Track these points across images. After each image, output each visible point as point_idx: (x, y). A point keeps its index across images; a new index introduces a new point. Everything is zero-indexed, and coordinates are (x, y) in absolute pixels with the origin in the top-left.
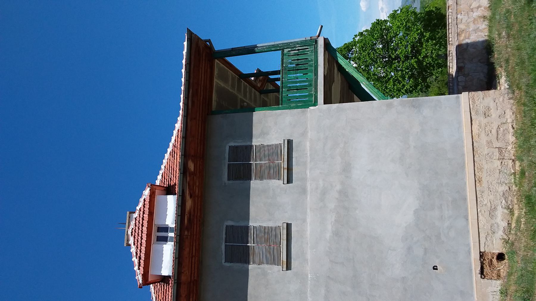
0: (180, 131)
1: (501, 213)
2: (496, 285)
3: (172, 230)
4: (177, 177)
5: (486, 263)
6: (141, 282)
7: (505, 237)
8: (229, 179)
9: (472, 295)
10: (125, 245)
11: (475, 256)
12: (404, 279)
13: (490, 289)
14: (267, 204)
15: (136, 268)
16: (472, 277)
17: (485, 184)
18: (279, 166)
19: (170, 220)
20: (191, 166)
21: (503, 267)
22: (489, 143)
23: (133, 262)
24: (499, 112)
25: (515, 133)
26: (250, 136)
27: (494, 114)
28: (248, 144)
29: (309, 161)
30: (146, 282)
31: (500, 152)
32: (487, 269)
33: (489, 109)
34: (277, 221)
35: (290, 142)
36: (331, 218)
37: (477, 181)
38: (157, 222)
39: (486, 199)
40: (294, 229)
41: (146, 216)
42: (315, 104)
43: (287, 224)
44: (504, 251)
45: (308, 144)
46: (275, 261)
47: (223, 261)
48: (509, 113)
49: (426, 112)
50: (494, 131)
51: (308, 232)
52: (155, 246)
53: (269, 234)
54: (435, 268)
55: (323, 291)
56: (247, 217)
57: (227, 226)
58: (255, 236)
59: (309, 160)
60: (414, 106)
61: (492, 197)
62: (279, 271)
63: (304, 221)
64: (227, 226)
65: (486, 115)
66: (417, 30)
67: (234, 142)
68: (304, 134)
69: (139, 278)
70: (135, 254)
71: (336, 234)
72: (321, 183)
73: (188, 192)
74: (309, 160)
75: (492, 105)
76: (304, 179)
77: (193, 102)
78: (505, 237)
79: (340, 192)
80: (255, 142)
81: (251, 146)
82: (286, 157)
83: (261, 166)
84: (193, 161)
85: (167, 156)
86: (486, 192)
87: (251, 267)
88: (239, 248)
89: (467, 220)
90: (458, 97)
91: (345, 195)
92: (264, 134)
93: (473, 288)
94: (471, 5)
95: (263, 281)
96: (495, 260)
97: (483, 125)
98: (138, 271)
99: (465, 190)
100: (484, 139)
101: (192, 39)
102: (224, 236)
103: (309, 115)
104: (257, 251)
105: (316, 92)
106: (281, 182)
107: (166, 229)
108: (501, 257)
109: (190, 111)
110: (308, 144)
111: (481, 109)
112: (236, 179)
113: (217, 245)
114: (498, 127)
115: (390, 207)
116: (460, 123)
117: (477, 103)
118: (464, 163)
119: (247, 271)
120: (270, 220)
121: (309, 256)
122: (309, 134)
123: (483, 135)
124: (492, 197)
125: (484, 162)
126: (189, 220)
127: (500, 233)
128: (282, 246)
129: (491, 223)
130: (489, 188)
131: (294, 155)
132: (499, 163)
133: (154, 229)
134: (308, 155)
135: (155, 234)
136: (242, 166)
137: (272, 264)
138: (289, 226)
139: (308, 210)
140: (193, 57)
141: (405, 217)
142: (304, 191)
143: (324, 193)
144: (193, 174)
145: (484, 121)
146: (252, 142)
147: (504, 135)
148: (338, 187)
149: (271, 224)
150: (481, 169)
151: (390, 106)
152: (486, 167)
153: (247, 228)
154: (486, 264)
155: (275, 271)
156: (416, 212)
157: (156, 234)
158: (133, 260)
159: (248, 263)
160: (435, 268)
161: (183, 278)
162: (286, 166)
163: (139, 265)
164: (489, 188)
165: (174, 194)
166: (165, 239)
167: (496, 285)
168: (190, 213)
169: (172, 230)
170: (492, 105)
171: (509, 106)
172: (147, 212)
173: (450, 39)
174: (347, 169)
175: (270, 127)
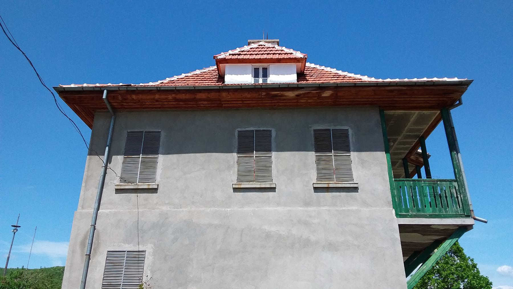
6: (219, 57)
8: (315, 131)
10: (249, 41)
14: (293, 168)
15: (230, 52)
18: (330, 179)
20: (327, 94)
23: (235, 49)
26: (359, 149)
28: (352, 148)
29: (337, 209)
30: (219, 62)
35: (355, 189)
38: (272, 67)
40: (271, 194)
41: (277, 56)
42: (398, 215)
43: (275, 188)
45: (354, 208)
47: (239, 130)
51: (268, 208)
52: (250, 67)
55: (216, 222)
57: (270, 131)
62: (232, 181)
63: (279, 204)
64: (270, 131)
67: (352, 134)
68: (365, 204)
69: (222, 56)
70: (242, 50)
71: (268, 236)
72: (316, 221)
73: (302, 92)
80: (354, 155)
82: (340, 186)
83: (330, 161)
84: (332, 95)
85: (334, 71)
87: (235, 155)
88: (253, 143)
91: (306, 244)
92: (363, 163)
98: (228, 54)
102: (261, 129)
103: (386, 208)
104: (247, 160)
110: (354, 208)
119: (229, 151)
121: (246, 209)
126: (276, 96)
128: (255, 184)
131: (343, 194)
133: (265, 65)
134: (344, 208)
135: (260, 66)
139: (289, 208)
140: (441, 88)
142: (307, 203)
143: (307, 224)
144: (319, 96)
146: (354, 151)
148: (313, 238)
159: (238, 153)
161: (224, 94)
162: (331, 186)
163: (233, 55)
168: (282, 96)
174: (332, 247)
175: (371, 169)
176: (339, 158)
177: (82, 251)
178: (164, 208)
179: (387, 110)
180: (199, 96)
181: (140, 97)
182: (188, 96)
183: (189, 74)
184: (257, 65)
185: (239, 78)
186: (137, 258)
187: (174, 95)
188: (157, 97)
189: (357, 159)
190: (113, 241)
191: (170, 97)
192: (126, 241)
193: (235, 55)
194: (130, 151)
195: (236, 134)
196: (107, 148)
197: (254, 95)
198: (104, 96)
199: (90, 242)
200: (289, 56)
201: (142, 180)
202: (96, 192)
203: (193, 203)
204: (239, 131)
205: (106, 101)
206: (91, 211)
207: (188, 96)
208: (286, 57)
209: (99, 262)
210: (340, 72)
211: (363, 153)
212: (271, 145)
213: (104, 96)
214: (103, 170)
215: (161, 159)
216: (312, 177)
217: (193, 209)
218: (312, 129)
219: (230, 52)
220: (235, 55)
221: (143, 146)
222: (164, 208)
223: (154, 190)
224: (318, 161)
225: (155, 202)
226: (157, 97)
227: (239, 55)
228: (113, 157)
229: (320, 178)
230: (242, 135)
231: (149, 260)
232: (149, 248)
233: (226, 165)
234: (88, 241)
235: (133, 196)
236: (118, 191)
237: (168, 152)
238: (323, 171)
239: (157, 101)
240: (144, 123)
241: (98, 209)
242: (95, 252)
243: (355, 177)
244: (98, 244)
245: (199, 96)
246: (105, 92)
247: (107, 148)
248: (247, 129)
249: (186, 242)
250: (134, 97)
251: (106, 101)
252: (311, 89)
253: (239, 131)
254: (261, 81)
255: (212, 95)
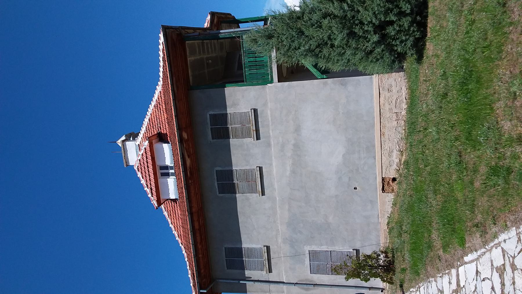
1: (395, 155)
2: (391, 197)
3: (171, 168)
5: (386, 183)
7: (398, 168)
9: (377, 202)
10: (125, 166)
11: (379, 180)
12: (336, 196)
13: (387, 199)
14: (243, 155)
15: (150, 195)
17: (386, 136)
19: (168, 161)
20: (185, 135)
21: (395, 186)
22: (391, 109)
24: (398, 88)
25: (407, 103)
27: (394, 90)
28: (224, 112)
29: (271, 124)
31: (397, 116)
32: (386, 187)
33: (391, 86)
34: (253, 165)
35: (255, 111)
37: (382, 134)
38: (159, 163)
39: (386, 147)
40: (264, 170)
41: (150, 161)
42: (271, 82)
43: (260, 167)
45: (269, 112)
46: (253, 191)
48: (404, 89)
49: (350, 88)
50: (394, 102)
51: (275, 172)
52: (161, 180)
53: (247, 174)
54: (355, 188)
55: (287, 207)
56: (230, 164)
60: (342, 84)
61: (390, 145)
62: (257, 197)
63: (271, 164)
68: (265, 104)
69: (155, 203)
71: (293, 172)
72: (281, 139)
75: (393, 83)
77: (177, 87)
78: (398, 168)
80: (229, 111)
82: (254, 122)
83: (236, 128)
85: (152, 107)
86: (387, 141)
88: (227, 184)
89: (375, 159)
90: (372, 78)
91: (297, 147)
92: (235, 105)
93: (377, 199)
96: (391, 182)
97: (387, 98)
98: (152, 198)
101: (166, 29)
102: (216, 177)
103: (267, 90)
104: (240, 186)
105: (272, 72)
107: (167, 168)
108: (394, 180)
110: (269, 112)
111: (387, 87)
112: (219, 138)
114: (397, 99)
115: (328, 153)
116: (372, 96)
117: (384, 82)
118: (374, 125)
121: (276, 186)
122: (269, 104)
123: (387, 104)
124: (390, 145)
125: (386, 122)
127: (395, 166)
128: (259, 181)
129: (389, 157)
130: (389, 139)
132: (396, 122)
133: (158, 168)
135: (159, 172)
136: (221, 129)
138: (261, 169)
139: (273, 158)
141: (337, 159)
142: (269, 145)
143: (283, 146)
144: (187, 141)
145: (388, 95)
147: (400, 104)
148: (293, 142)
150: (385, 127)
151: (325, 84)
152: (388, 125)
153: (232, 171)
155: (255, 197)
156: (343, 156)
161: (194, 210)
162: (254, 129)
163: (152, 194)
164: (389, 139)
166: (168, 175)
167: (391, 197)
168: (190, 168)
169: (171, 168)
170: (393, 83)
174: (298, 129)
175: (239, 99)
177: (311, 289)
178: (280, 240)
179: (189, 82)
180: (197, 227)
181: (202, 267)
182: (198, 235)
183: (169, 220)
184: (159, 175)
185: (172, 187)
186: (313, 255)
187: (198, 245)
188: (200, 256)
190: (304, 272)
191: (200, 247)
192: (303, 262)
194: (242, 267)
196: (241, 282)
198: (205, 291)
199: (305, 285)
200: (148, 149)
201: (262, 257)
202: (272, 286)
203: (275, 222)
205: (208, 289)
206: (285, 287)
207: (198, 235)
209: (318, 278)
211: (227, 104)
213: (205, 291)
214: (256, 283)
215: (245, 245)
216: (250, 141)
217: (279, 222)
218: (212, 140)
221: (236, 257)
222: (280, 240)
223: (268, 248)
224: (236, 137)
225: (276, 247)
226: (200, 256)
231: (315, 248)
232: (307, 249)
233: (246, 203)
234: (305, 286)
235: (273, 261)
236: (270, 271)
237: (240, 242)
238: (244, 134)
239: (203, 254)
240: (220, 259)
241: (283, 283)
242: (312, 281)
244: (306, 280)
245: (197, 227)
246: (201, 291)
247: (241, 282)
248: (217, 187)
249: (302, 225)
250: (202, 271)
251: (208, 289)
255: (195, 218)
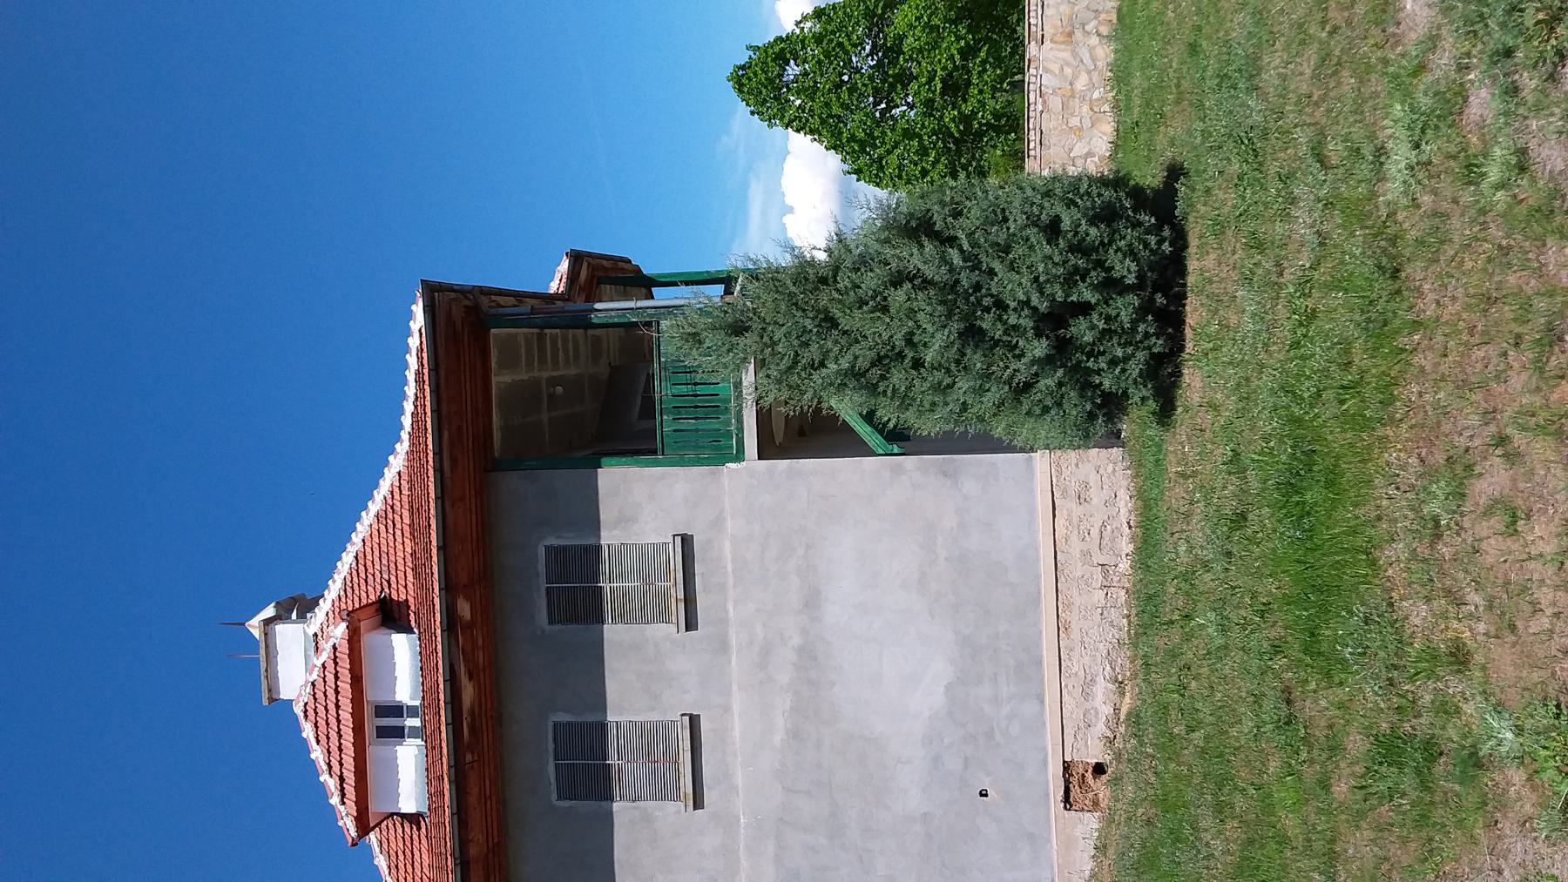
0: (405, 477)
2: (1089, 823)
3: (413, 711)
4: (410, 585)
5: (1074, 780)
6: (353, 833)
8: (551, 622)
9: (1049, 841)
10: (265, 702)
11: (1055, 770)
13: (1079, 831)
14: (643, 675)
15: (335, 800)
16: (1049, 808)
17: (1075, 634)
18: (665, 594)
19: (405, 690)
20: (464, 609)
21: (1101, 787)
22: (1087, 554)
23: (323, 785)
24: (1106, 493)
25: (1133, 539)
26: (595, 525)
27: (1097, 497)
28: (591, 541)
30: (364, 827)
31: (1106, 574)
32: (1075, 791)
34: (671, 710)
35: (687, 541)
36: (783, 703)
37: (1061, 628)
38: (373, 695)
39: (1074, 665)
40: (705, 726)
42: (739, 457)
44: (1106, 758)
45: (727, 546)
46: (667, 792)
47: (554, 796)
48: (1124, 496)
49: (970, 486)
50: (1095, 532)
51: (737, 733)
52: (375, 750)
53: (651, 736)
54: (983, 794)
55: (771, 847)
57: (556, 725)
58: (621, 742)
59: (731, 582)
60: (945, 474)
62: (679, 812)
63: (727, 709)
64: (556, 725)
65: (1081, 499)
66: (958, 39)
67: (559, 537)
68: (718, 523)
70: (325, 767)
71: (795, 734)
72: (759, 630)
73: (463, 669)
74: (731, 582)
75: (1093, 479)
76: (723, 622)
77: (454, 461)
79: (800, 650)
80: (608, 538)
81: (598, 548)
84: (467, 598)
85: (368, 518)
87: (617, 806)
88: (586, 768)
89: (1042, 702)
91: (808, 656)
92: (625, 520)
93: (1049, 827)
94: (1071, 150)
95: (643, 830)
96: (1089, 775)
97: (1075, 520)
98: (342, 808)
99: (1039, 646)
100: (1076, 547)
101: (434, 293)
102: (551, 746)
104: (627, 778)
105: (741, 429)
106: (673, 628)
107: (397, 710)
108: (1099, 769)
109: (448, 482)
110: (727, 546)
111: (1074, 488)
113: (537, 765)
115: (900, 679)
116: (1032, 512)
117: (1066, 473)
119: (608, 818)
120: (653, 709)
121: (739, 780)
122: (729, 524)
123: (1074, 538)
125: (1075, 593)
126: (472, 728)
127: (1100, 728)
128: (686, 762)
129: (1084, 703)
130: (1083, 642)
131: (699, 569)
132: (1102, 594)
133: (368, 711)
134: (730, 569)
135: (371, 723)
136: (579, 592)
137: (663, 799)
138: (694, 721)
139: (735, 687)
140: (441, 351)
142: (723, 647)
143: (766, 651)
144: (471, 625)
145: (1078, 511)
146: (599, 537)
147: (1113, 540)
148: (796, 640)
149: (654, 717)
150: (1069, 605)
151: (898, 471)
152: (1077, 601)
154: (1075, 783)
155: (671, 813)
156: (949, 687)
157: (378, 723)
158: (322, 779)
159: (610, 799)
160: (983, 794)
161: (473, 851)
162: (681, 595)
163: (343, 795)
164: (1083, 642)
165: (409, 631)
166: (398, 733)
167: (1089, 823)
168: (472, 713)
170: (1093, 479)
171: (1124, 483)
172: (345, 675)
173: (1032, 145)
174: (812, 602)
175: (639, 505)
176: (616, 571)
185: (408, 775)
189: (615, 532)
193: (342, 790)
195: (566, 804)
197: (473, 778)
204: (559, 798)
208: (345, 663)
210: (375, 507)
212: (590, 725)
218: (547, 627)
219: (335, 800)
220: (342, 790)
224: (623, 617)
227: (342, 779)
228: (419, 742)
229: (663, 617)
230: (568, 790)
238: (649, 608)
243: (653, 539)
248: (553, 780)
252: (454, 649)
253: (559, 798)
254: (415, 722)
